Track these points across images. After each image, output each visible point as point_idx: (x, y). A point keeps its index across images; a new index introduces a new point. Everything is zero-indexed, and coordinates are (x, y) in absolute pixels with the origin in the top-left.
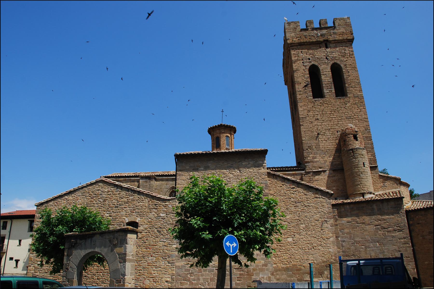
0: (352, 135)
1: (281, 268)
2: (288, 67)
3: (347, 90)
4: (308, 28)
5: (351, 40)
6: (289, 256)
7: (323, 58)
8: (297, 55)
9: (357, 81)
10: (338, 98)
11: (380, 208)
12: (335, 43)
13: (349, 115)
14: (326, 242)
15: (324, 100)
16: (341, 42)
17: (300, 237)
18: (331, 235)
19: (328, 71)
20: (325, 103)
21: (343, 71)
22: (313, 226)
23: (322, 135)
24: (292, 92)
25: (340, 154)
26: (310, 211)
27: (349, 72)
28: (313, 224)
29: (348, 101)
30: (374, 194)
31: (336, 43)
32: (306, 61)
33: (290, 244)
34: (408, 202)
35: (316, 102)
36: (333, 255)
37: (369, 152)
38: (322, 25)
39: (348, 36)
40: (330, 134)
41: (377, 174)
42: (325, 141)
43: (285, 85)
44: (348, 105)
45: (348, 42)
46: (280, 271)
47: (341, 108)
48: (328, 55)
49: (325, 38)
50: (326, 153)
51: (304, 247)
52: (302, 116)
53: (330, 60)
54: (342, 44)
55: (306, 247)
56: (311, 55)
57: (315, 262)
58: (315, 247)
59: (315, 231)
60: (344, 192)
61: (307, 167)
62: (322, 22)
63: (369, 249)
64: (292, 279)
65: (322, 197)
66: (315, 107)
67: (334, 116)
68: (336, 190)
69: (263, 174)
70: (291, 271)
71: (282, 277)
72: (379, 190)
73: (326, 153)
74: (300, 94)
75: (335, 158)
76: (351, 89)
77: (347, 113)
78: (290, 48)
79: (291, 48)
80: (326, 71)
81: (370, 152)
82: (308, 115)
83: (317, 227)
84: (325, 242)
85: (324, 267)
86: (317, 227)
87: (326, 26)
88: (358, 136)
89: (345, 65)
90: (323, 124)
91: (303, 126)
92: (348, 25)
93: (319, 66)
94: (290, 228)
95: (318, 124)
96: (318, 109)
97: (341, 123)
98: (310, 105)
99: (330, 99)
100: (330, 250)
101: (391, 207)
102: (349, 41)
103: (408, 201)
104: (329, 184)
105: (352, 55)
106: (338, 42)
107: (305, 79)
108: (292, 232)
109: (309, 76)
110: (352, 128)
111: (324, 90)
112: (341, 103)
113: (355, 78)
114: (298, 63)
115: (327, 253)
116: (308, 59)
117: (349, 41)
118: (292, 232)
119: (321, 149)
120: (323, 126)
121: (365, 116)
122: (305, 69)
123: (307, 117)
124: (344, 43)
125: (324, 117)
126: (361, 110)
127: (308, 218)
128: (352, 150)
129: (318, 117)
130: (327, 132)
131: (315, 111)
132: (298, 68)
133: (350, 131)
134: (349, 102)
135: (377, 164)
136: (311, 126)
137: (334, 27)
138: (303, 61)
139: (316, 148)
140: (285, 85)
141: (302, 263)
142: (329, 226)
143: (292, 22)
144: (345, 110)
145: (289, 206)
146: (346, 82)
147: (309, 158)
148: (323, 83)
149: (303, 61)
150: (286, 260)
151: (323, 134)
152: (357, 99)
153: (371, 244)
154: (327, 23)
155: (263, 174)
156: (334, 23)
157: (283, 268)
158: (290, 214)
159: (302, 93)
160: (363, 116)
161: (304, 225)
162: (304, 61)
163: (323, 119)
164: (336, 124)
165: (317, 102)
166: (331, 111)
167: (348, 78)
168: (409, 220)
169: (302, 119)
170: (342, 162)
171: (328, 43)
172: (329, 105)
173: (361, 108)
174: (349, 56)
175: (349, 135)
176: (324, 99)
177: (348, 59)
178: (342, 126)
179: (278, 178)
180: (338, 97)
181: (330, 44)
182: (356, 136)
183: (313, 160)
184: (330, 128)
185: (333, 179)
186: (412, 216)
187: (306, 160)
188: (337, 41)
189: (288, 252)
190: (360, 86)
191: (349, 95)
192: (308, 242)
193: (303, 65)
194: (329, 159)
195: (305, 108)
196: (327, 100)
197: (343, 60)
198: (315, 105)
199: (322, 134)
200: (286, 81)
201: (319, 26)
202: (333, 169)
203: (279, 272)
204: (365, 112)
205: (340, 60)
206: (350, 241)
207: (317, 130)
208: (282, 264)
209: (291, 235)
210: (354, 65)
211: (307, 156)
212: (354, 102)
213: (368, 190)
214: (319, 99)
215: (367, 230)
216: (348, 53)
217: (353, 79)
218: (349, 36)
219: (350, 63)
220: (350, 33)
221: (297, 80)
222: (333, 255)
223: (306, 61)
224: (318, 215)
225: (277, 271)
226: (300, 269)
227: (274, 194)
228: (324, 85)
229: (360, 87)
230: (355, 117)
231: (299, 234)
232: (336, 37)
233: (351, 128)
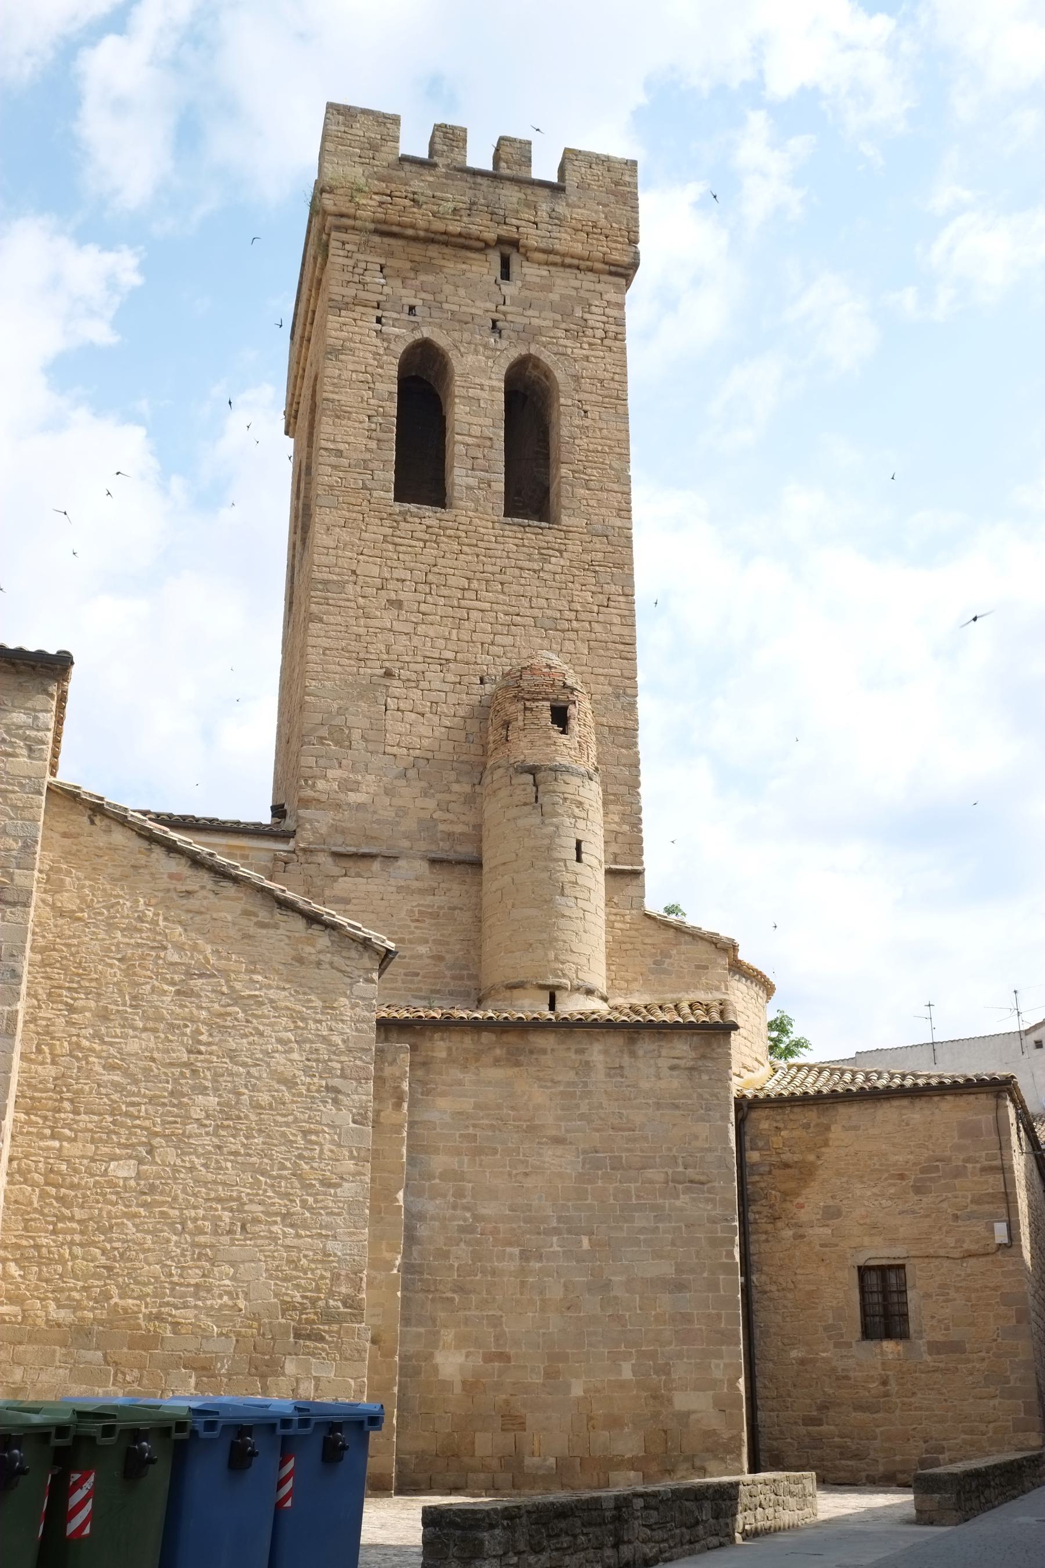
0: (548, 704)
1: (43, 1326)
2: (309, 340)
3: (563, 493)
4: (436, 159)
5: (620, 270)
6: (103, 1260)
7: (477, 320)
8: (356, 278)
9: (615, 464)
10: (514, 524)
11: (621, 1067)
12: (547, 264)
13: (549, 613)
14: (316, 1201)
15: (443, 517)
16: (578, 268)
17: (179, 1162)
18: (350, 1165)
19: (492, 389)
20: (449, 532)
21: (562, 401)
22: (262, 1108)
23: (408, 684)
24: (304, 465)
25: (478, 788)
26: (261, 1028)
27: (586, 412)
28: (264, 1098)
29: (557, 546)
30: (605, 999)
31: (555, 264)
32: (395, 315)
33: (117, 1193)
34: (756, 1064)
35: (405, 520)
36: (343, 1273)
37: (612, 802)
38: (503, 164)
39: (614, 245)
40: (447, 687)
41: (634, 912)
42: (413, 716)
43: (287, 433)
44: (557, 563)
45: (611, 273)
46: (32, 1339)
47: (517, 572)
48: (505, 314)
49: (503, 231)
50: (412, 773)
51: (195, 1220)
52: (326, 576)
53: (509, 337)
54: (580, 276)
55: (204, 1218)
56: (424, 295)
57: (242, 1303)
58: (256, 1221)
59: (269, 1136)
60: (465, 972)
61: (308, 826)
62: (506, 149)
63: (538, 1265)
64: (101, 1391)
65: (331, 964)
66: (396, 545)
67: (477, 604)
68: (428, 961)
69: (22, 785)
70: (97, 1349)
71: (44, 1377)
72: (635, 986)
73: (412, 773)
74: (334, 467)
75: (452, 806)
76: (582, 491)
77: (543, 602)
78: (329, 235)
79: (334, 234)
80: (481, 385)
81: (618, 799)
82: (354, 572)
83: (280, 1119)
84: (311, 1200)
85: (287, 1333)
86: (285, 1116)
87: (522, 174)
88: (572, 710)
89: (577, 378)
90: (421, 629)
91: (321, 621)
92: (623, 195)
93: (453, 356)
94: (133, 1104)
95: (398, 626)
96: (407, 558)
97: (508, 640)
98: (377, 530)
99: (476, 521)
100: (330, 1245)
101: (673, 1068)
102: (613, 269)
103: (757, 1060)
104: (400, 927)
105: (616, 339)
106: (564, 265)
107: (372, 401)
108: (142, 1128)
109: (395, 388)
110: (550, 667)
111: (457, 471)
112: (525, 549)
113: (610, 447)
114: (355, 315)
115: (313, 1261)
116: (406, 309)
117: (613, 269)
118: (142, 1128)
119: (389, 749)
120: (416, 641)
121: (626, 631)
122: (381, 351)
123: (348, 582)
124: (591, 276)
125: (429, 599)
126: (609, 599)
127: (244, 1065)
128: (533, 770)
129: (402, 596)
130: (434, 677)
131: (396, 564)
132: (351, 340)
133: (539, 679)
134: (560, 551)
135: (641, 863)
136: (362, 631)
137: (556, 189)
138: (379, 313)
139: (366, 740)
140: (287, 433)
141: (168, 1304)
142: (346, 1119)
143: (365, 112)
144: (537, 582)
145: (148, 987)
146: (564, 457)
147: (321, 785)
148: (458, 437)
149: (379, 313)
150: (80, 1284)
151: (414, 677)
152: (599, 544)
153: (555, 1239)
154: (527, 161)
155: (22, 785)
156: (562, 170)
157: (59, 1325)
158: (145, 1029)
159: (345, 462)
160: (616, 630)
161: (213, 1100)
162: (385, 314)
163: (423, 607)
164: (482, 644)
165: (410, 519)
166: (470, 574)
167: (577, 442)
168: (748, 1145)
169: (320, 586)
170: (478, 827)
171: (515, 259)
172: (465, 549)
173: (613, 589)
174: (602, 339)
175: (534, 700)
176: (446, 514)
177: (592, 353)
178: (509, 655)
179: (120, 829)
180: (516, 520)
181: (525, 263)
182: (566, 708)
183: (342, 796)
184: (450, 655)
185: (421, 902)
186: (764, 1125)
187: (308, 793)
188: (558, 259)
189: (103, 1238)
190: (625, 489)
191: (565, 519)
192: (222, 1192)
193: (379, 332)
194: (419, 802)
195: (345, 537)
196: (460, 519)
197: (569, 351)
198: (398, 533)
199: (408, 680)
200: (290, 415)
201: (489, 166)
202: (433, 855)
203: (30, 1348)
204: (627, 613)
205: (555, 349)
206: (453, 1218)
207: (385, 657)
208: (52, 1305)
209: (133, 1146)
210: (616, 385)
211: (317, 771)
212: (587, 557)
213: (581, 975)
214: (427, 510)
215: (547, 1165)
216: (598, 325)
217: (600, 448)
218: (619, 246)
219: (601, 374)
220: (622, 236)
221: (336, 397)
222: (343, 1273)
223: (395, 315)
224: (295, 1056)
225: (20, 1343)
226: (149, 1342)
227: (79, 915)
228: (459, 449)
229: (623, 493)
230: (575, 624)
231: (181, 1143)
232: (558, 235)
233: (547, 670)
